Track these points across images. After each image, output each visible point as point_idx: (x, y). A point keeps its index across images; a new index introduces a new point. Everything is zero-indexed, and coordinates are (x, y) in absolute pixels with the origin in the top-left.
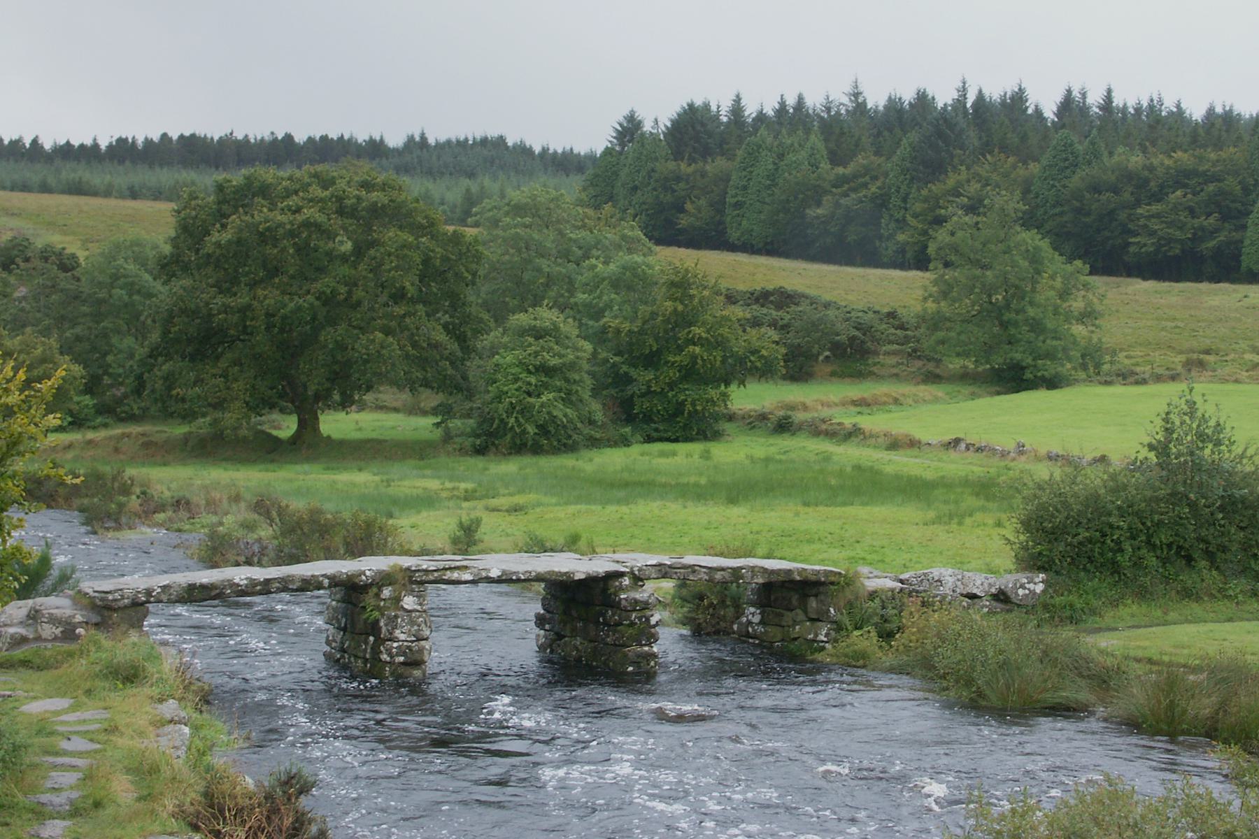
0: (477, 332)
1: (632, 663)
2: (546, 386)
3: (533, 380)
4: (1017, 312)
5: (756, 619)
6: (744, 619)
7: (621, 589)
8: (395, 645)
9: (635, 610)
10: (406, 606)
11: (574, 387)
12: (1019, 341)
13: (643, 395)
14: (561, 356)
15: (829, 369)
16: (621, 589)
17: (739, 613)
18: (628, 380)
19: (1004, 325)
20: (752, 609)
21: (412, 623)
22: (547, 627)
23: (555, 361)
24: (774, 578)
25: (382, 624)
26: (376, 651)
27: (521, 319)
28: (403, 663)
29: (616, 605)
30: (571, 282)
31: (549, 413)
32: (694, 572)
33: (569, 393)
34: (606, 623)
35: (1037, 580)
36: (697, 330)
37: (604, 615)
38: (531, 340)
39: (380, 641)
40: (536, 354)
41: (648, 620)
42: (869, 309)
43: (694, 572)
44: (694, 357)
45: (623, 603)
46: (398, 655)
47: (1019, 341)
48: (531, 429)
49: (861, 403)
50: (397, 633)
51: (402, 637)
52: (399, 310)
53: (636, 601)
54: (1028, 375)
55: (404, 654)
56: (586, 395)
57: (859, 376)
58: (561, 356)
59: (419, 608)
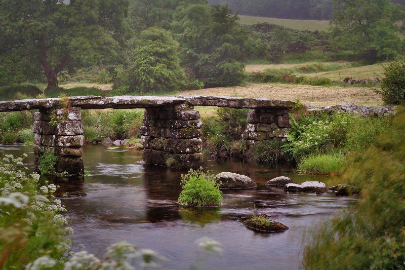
0: (129, 37)
1: (189, 147)
2: (157, 61)
3: (152, 58)
4: (373, 28)
5: (253, 129)
6: (247, 131)
7: (182, 109)
8: (65, 137)
9: (189, 120)
10: (70, 118)
11: (172, 62)
12: (373, 40)
13: (203, 65)
14: (165, 48)
15: (287, 57)
16: (182, 109)
17: (244, 126)
18: (196, 59)
19: (367, 34)
20: (251, 125)
21: (73, 126)
22: (146, 134)
23: (162, 50)
24: (261, 105)
25: (58, 127)
26: (56, 142)
27: (147, 32)
28: (69, 147)
29: (179, 118)
30: (171, 17)
31: (161, 73)
32: (219, 101)
33: (170, 64)
34: (175, 128)
35: (393, 109)
36: (229, 36)
37: (173, 123)
38: (151, 41)
39: (58, 136)
40: (153, 48)
41: (196, 124)
42: (306, 31)
43: (219, 101)
44: (227, 48)
45: (183, 116)
46: (67, 142)
47: (373, 40)
48: (152, 81)
49: (304, 70)
50: (66, 131)
51: (69, 133)
52: (91, 27)
53: (190, 115)
54: (378, 55)
55: (70, 142)
56: (177, 65)
57: (301, 59)
58: (165, 48)
59: (77, 118)
